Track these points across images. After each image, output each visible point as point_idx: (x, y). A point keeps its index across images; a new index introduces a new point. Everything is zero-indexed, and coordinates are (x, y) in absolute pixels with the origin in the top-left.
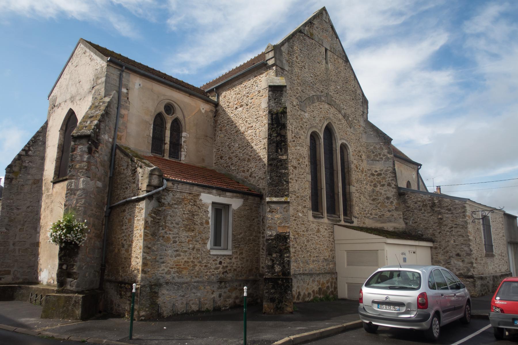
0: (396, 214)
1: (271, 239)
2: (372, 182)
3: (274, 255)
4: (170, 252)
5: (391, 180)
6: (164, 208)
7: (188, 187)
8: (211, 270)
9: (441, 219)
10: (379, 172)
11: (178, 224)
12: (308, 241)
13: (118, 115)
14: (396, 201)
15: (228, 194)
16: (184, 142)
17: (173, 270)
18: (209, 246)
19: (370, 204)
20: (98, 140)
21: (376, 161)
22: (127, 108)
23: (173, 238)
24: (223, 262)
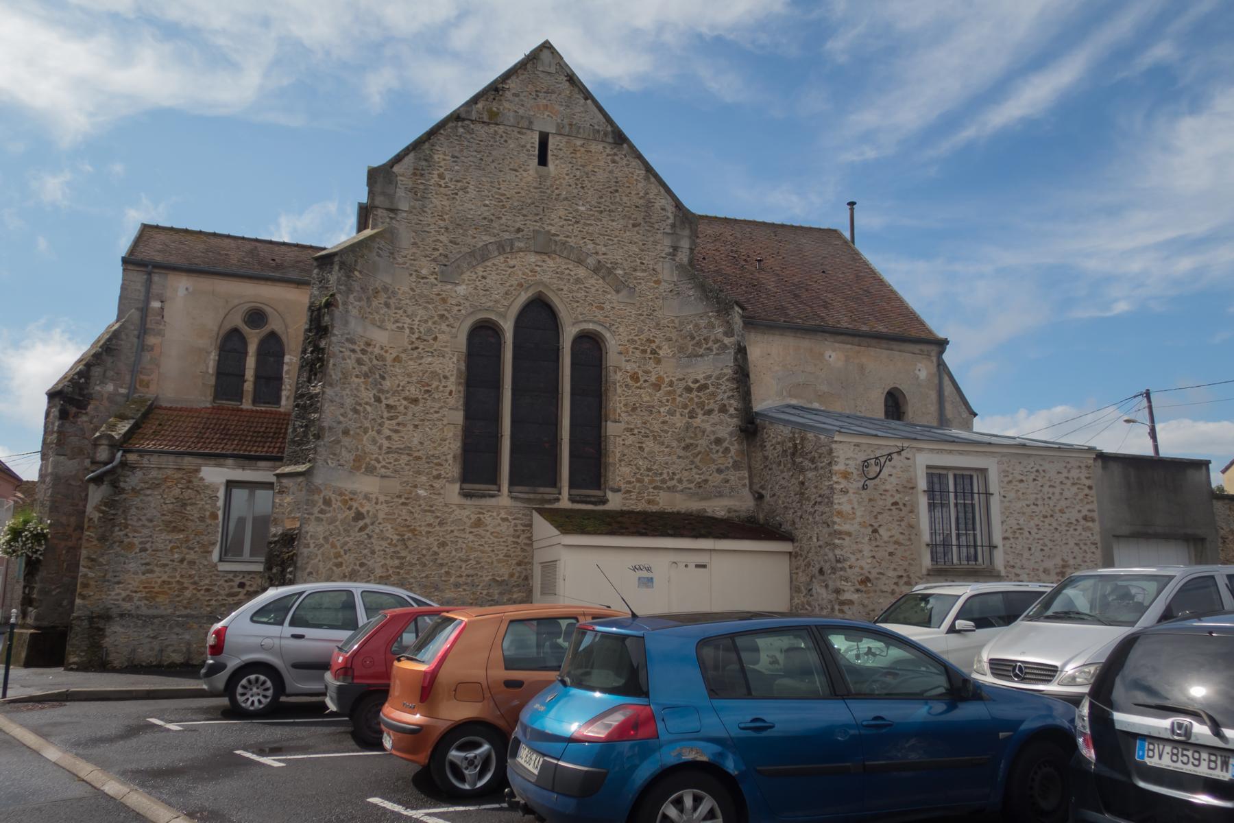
0: (733, 476)
1: (275, 542)
2: (685, 407)
3: (274, 571)
4: (132, 566)
5: (729, 398)
6: (124, 496)
7: (172, 458)
8: (220, 598)
9: (802, 483)
10: (702, 382)
11: (151, 521)
12: (443, 544)
13: (143, 347)
14: (736, 446)
15: (262, 464)
16: (287, 372)
17: (139, 595)
18: (215, 556)
19: (679, 457)
20: (83, 396)
21: (697, 356)
22: (160, 333)
23: (141, 543)
24: (248, 583)
